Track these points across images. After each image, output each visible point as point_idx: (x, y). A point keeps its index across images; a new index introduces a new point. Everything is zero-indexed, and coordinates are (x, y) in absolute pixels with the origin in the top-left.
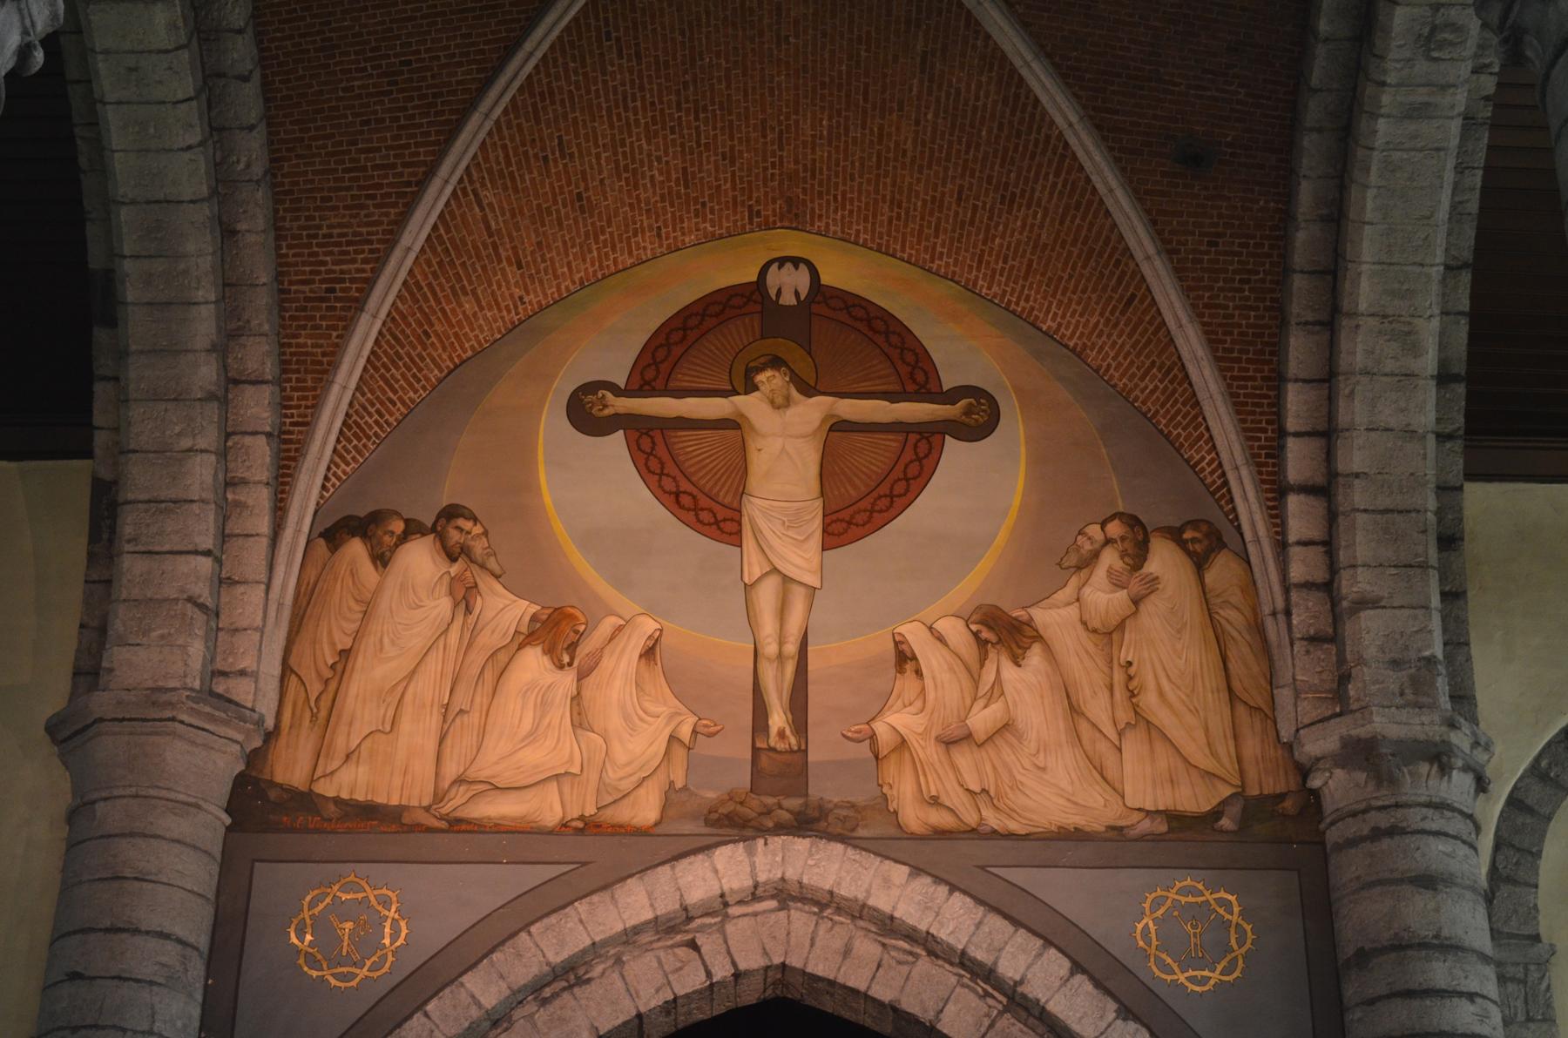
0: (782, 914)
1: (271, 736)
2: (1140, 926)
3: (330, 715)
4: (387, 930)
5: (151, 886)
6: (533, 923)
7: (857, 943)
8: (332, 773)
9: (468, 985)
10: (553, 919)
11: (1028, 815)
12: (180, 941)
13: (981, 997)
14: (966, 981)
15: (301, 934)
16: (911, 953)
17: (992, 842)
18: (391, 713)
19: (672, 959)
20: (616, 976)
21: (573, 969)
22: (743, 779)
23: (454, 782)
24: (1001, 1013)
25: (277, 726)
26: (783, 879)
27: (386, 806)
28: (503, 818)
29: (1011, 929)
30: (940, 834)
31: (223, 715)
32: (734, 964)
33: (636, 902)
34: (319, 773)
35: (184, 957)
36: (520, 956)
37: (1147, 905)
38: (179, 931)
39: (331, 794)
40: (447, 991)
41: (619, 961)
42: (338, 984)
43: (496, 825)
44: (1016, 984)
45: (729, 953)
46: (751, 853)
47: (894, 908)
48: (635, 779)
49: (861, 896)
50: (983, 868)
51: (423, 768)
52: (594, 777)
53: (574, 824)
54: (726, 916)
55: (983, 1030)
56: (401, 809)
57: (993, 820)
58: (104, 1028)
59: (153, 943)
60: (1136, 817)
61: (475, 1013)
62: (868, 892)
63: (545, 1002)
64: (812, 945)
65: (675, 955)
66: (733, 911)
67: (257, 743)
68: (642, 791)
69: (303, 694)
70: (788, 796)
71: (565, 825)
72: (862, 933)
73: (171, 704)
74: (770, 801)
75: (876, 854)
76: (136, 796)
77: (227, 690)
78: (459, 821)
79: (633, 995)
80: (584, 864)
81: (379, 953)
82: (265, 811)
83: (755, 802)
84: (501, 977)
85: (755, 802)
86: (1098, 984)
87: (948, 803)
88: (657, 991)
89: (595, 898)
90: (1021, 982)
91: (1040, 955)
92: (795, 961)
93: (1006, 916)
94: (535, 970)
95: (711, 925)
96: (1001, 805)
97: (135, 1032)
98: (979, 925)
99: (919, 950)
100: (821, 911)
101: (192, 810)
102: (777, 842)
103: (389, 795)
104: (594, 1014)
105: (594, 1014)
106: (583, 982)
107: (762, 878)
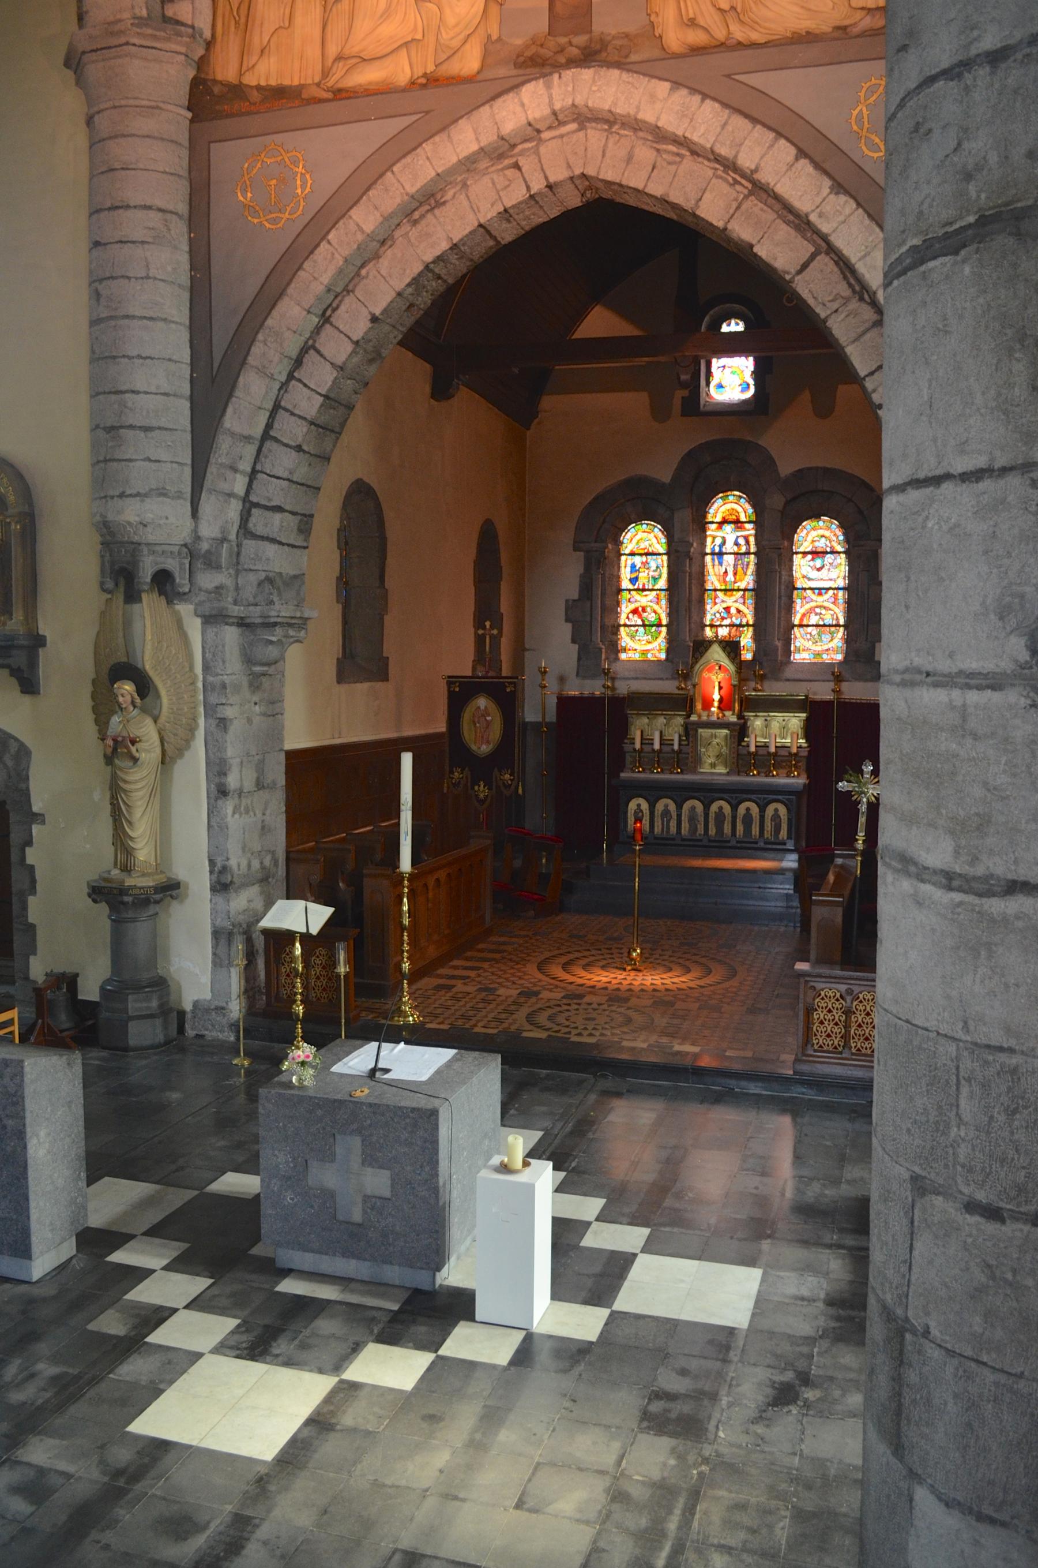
0: (581, 134)
1: (209, 45)
2: (855, 113)
3: (247, 21)
4: (298, 182)
5: (133, 172)
6: (394, 164)
7: (637, 150)
8: (253, 66)
9: (354, 217)
10: (408, 159)
11: (767, 25)
12: (160, 210)
13: (731, 185)
14: (719, 172)
15: (244, 192)
16: (678, 154)
17: (736, 54)
18: (288, 11)
19: (501, 178)
20: (463, 197)
21: (433, 195)
22: (542, 25)
23: (335, 60)
24: (746, 197)
25: (213, 36)
26: (573, 105)
27: (291, 87)
28: (370, 83)
29: (750, 126)
30: (696, 51)
31: (163, 34)
32: (546, 178)
33: (466, 138)
34: (244, 68)
35: (166, 221)
36: (387, 190)
37: (862, 94)
38: (159, 203)
39: (254, 83)
40: (341, 223)
41: (465, 185)
42: (271, 227)
43: (366, 90)
44: (752, 172)
45: (542, 170)
46: (548, 86)
47: (658, 119)
48: (462, 36)
49: (632, 113)
50: (729, 76)
51: (313, 52)
52: (431, 39)
53: (420, 81)
54: (540, 140)
55: (732, 211)
56: (302, 87)
57: (739, 33)
58: (116, 278)
59: (140, 214)
60: (859, 15)
61: (360, 237)
62: (638, 108)
63: (415, 222)
64: (603, 156)
65: (505, 175)
66: (545, 135)
67: (201, 52)
68: (467, 46)
69: (228, 7)
70: (576, 34)
71: (413, 83)
72: (640, 142)
73: (121, 32)
74: (563, 40)
75: (644, 75)
76: (115, 107)
77: (175, 14)
78: (340, 90)
79: (475, 210)
80: (427, 113)
81: (295, 200)
82: (212, 103)
83: (551, 43)
84: (376, 208)
85: (551, 43)
86: (817, 166)
87: (702, 23)
88: (492, 205)
89: (437, 138)
90: (756, 170)
91: (771, 146)
92: (591, 172)
93: (747, 116)
94: (398, 200)
95: (529, 149)
96: (746, 19)
97: (136, 278)
98: (724, 126)
99: (684, 152)
100: (610, 127)
101: (157, 111)
102: (568, 74)
103: (291, 79)
104: (450, 228)
105: (450, 228)
106: (440, 204)
107: (557, 106)
